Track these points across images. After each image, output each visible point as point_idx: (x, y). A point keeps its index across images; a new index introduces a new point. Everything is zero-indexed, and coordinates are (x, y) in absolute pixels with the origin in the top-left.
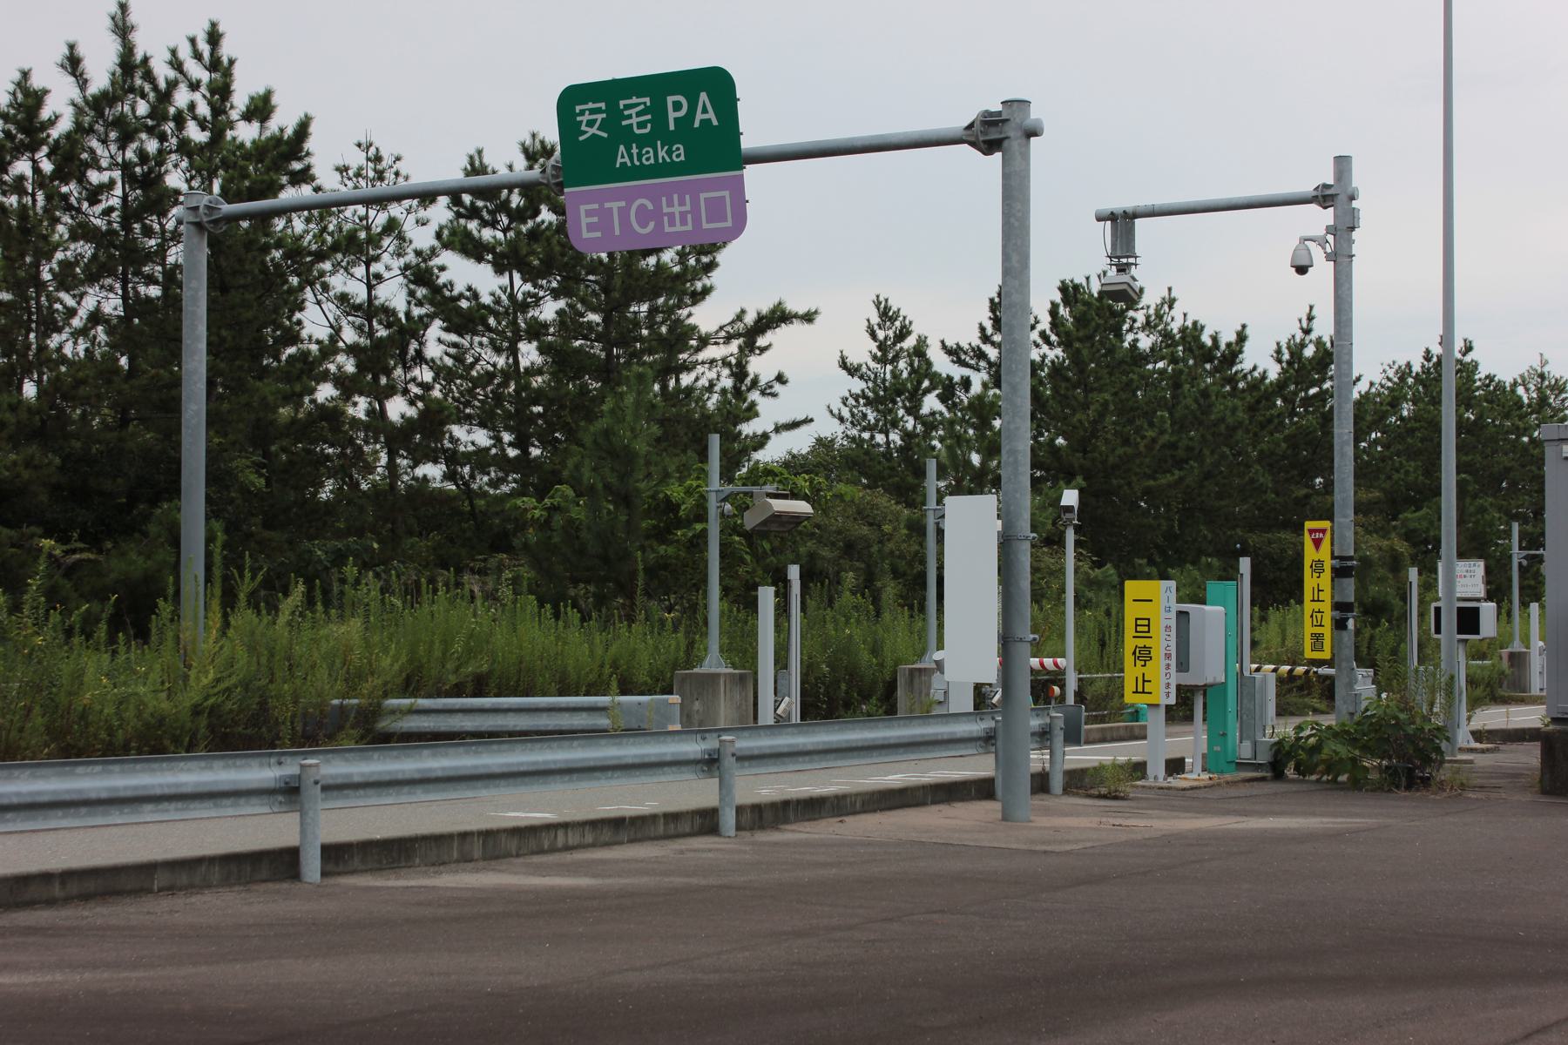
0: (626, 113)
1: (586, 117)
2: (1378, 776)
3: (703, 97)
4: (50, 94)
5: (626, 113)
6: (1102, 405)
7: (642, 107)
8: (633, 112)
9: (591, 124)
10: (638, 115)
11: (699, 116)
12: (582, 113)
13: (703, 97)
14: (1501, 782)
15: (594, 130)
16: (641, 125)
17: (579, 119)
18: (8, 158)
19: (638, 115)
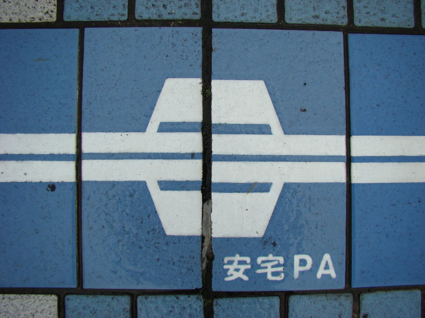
0: (262, 265)
1: (235, 265)
2: (302, 230)
3: (327, 257)
4: (323, 269)
5: (262, 265)
6: (308, 225)
7: (276, 263)
8: (269, 265)
9: (237, 270)
10: (273, 267)
11: (321, 272)
12: (230, 263)
13: (327, 257)
14: (206, 248)
15: (240, 275)
16: (274, 274)
17: (226, 267)
18: (279, 16)
19: (273, 267)
